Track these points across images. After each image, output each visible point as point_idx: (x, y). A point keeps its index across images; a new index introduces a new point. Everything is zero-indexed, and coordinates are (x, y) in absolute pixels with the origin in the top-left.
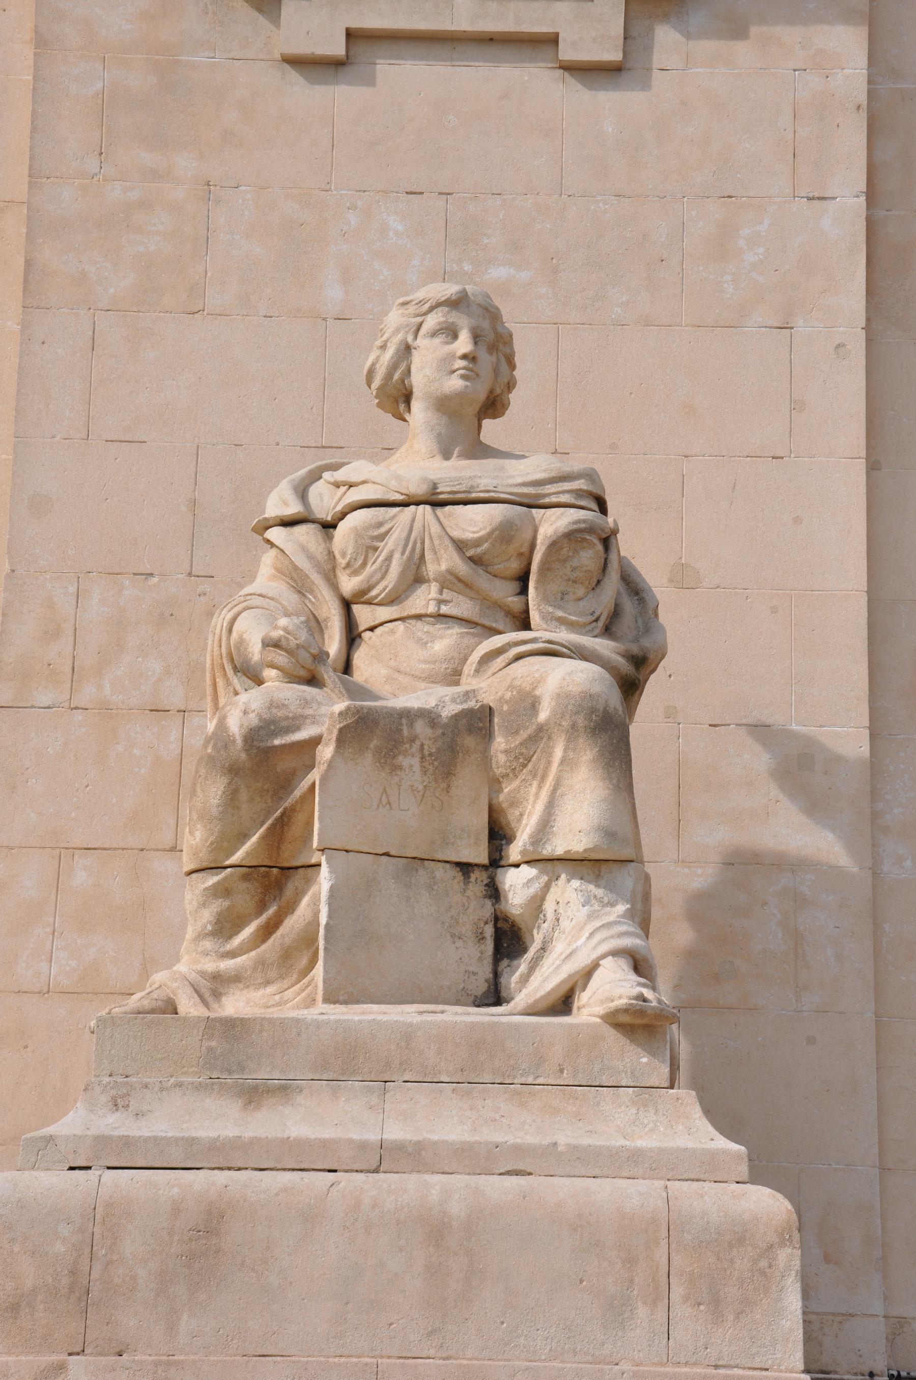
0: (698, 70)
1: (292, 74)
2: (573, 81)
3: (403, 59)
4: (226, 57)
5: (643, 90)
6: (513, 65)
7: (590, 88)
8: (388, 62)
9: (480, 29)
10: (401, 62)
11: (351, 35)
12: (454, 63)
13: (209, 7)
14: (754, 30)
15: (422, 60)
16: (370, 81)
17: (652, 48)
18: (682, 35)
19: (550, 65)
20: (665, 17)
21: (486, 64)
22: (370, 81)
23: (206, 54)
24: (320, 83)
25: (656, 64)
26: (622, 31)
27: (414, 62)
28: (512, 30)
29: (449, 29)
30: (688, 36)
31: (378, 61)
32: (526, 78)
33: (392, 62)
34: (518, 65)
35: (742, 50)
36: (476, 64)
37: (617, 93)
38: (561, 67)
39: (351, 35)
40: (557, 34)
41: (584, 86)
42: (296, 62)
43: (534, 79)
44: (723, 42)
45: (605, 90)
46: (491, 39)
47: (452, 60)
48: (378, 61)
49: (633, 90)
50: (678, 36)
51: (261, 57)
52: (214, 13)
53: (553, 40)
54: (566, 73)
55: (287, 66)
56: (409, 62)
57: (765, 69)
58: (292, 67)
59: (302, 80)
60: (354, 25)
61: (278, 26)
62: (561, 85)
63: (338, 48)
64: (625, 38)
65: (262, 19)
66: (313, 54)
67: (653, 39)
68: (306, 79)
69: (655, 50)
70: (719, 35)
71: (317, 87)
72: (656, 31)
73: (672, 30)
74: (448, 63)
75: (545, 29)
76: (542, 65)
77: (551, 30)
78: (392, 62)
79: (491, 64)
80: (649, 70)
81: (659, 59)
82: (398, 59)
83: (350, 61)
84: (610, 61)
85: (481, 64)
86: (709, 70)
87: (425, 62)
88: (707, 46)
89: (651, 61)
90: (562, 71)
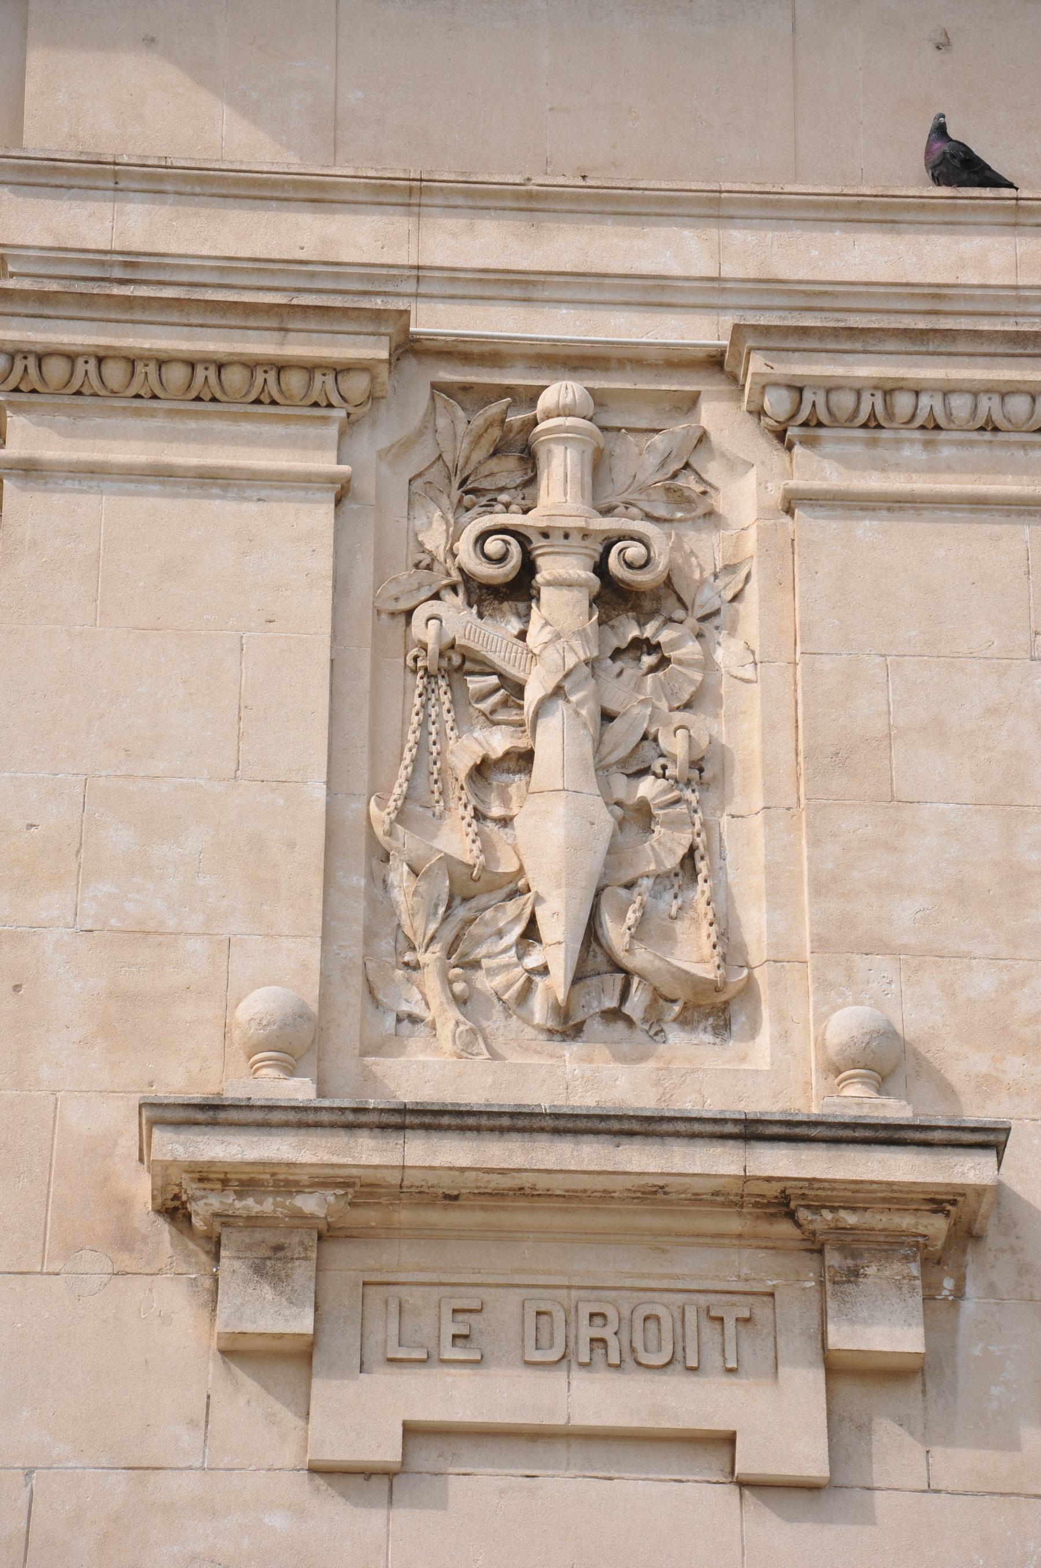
22: (441, 1504)
39: (411, 1431)
43: (700, 1500)
63: (388, 1450)
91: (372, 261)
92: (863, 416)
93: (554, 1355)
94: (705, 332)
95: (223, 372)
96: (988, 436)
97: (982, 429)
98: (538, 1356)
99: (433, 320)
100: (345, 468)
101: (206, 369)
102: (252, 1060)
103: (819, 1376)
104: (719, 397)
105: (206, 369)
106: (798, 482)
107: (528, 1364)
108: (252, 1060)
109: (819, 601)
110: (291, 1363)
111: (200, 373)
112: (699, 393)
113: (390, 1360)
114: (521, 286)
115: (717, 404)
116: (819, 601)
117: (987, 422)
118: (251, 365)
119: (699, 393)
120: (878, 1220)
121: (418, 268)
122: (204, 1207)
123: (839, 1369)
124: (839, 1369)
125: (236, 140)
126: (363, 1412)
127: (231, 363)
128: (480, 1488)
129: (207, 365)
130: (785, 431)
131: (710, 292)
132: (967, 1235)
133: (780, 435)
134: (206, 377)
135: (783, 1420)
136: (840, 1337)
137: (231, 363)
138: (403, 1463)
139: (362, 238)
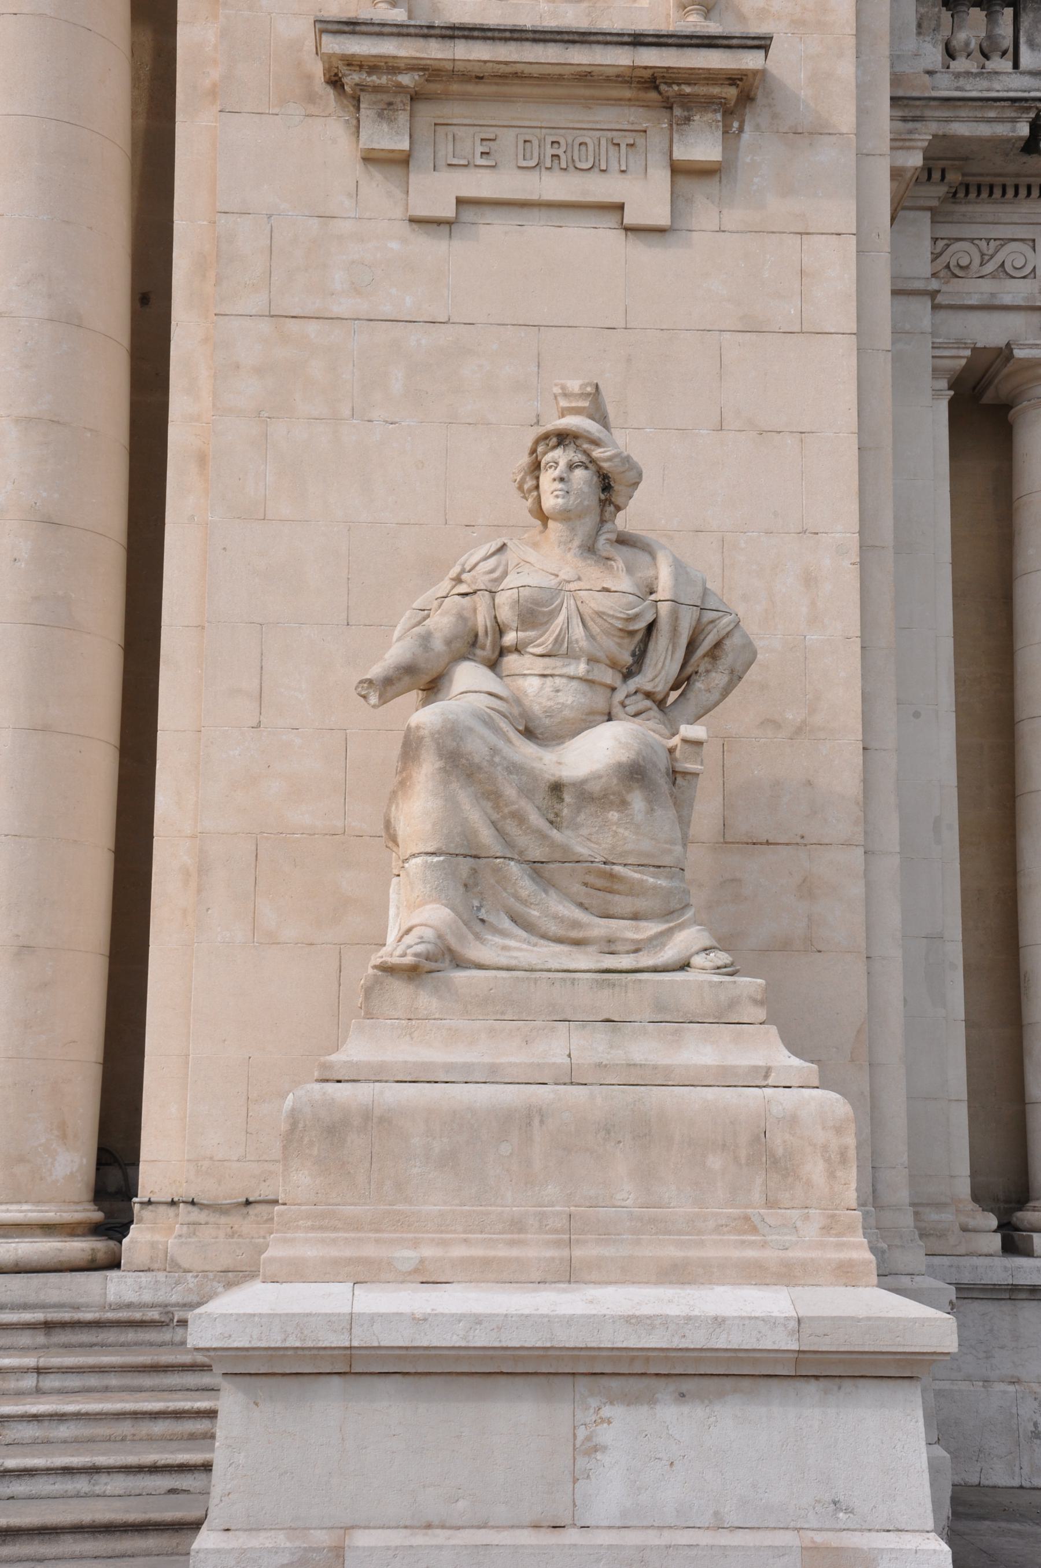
39: (460, 202)
43: (600, 238)
63: (448, 211)
126: (435, 191)
128: (495, 232)
132: (747, 98)
135: (648, 196)
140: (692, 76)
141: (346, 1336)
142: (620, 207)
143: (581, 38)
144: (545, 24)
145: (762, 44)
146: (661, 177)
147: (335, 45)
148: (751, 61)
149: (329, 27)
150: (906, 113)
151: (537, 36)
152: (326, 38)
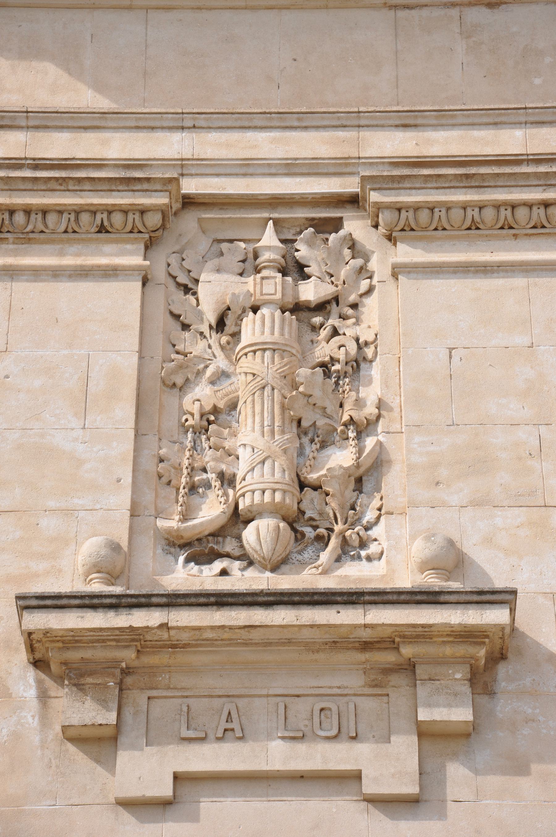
0: (488, 802)
1: (125, 815)
2: (377, 812)
3: (224, 796)
4: (66, 803)
5: (440, 819)
6: (322, 799)
7: (392, 818)
8: (211, 799)
9: (292, 769)
10: (222, 799)
11: (177, 777)
12: (269, 799)
13: (53, 761)
14: (535, 767)
15: (241, 796)
16: (195, 818)
17: (445, 783)
18: (470, 771)
19: (359, 798)
20: (454, 756)
21: (298, 798)
22: (195, 818)
23: (48, 802)
24: (149, 822)
25: (450, 797)
26: (417, 768)
27: (233, 799)
28: (319, 768)
29: (265, 769)
30: (477, 772)
31: (201, 800)
32: (334, 810)
33: (214, 799)
34: (326, 799)
35: (525, 784)
36: (289, 799)
37: (416, 823)
38: (365, 800)
39: (178, 778)
40: (360, 771)
41: (387, 816)
42: (128, 804)
43: (341, 811)
44: (508, 777)
45: (405, 819)
46: (302, 777)
47: (267, 796)
48: (201, 800)
49: (430, 819)
50: (467, 771)
51: (97, 801)
52: (58, 767)
53: (357, 776)
54: (370, 805)
55: (120, 808)
56: (229, 799)
57: (548, 802)
58: (124, 809)
59: (133, 820)
60: (181, 768)
61: (113, 773)
62: (366, 816)
63: (166, 790)
64: (420, 774)
65: (99, 769)
66: (144, 796)
67: (445, 775)
68: (128, 812)
69: (448, 784)
70: (504, 771)
71: (146, 825)
72: (448, 768)
73: (462, 767)
74: (264, 799)
75: (348, 767)
76: (348, 798)
77: (355, 768)
78: (214, 799)
79: (303, 799)
80: (444, 801)
81: (453, 791)
82: (219, 797)
83: (176, 801)
84: (409, 794)
85: (294, 799)
86: (498, 802)
87: (243, 799)
88: (494, 781)
89: (445, 794)
90: (366, 803)
91: (234, 157)
92: (468, 223)
93: (334, 732)
94: (349, 185)
95: (515, 210)
96: (440, 233)
97: (502, 228)
98: (191, 734)
99: (190, 186)
100: (148, 263)
101: (134, 214)
102: (90, 577)
103: (415, 738)
104: (352, 218)
105: (37, 214)
106: (400, 259)
107: (184, 739)
108: (90, 577)
109: (420, 321)
110: (100, 743)
111: (469, 212)
112: (341, 218)
113: (184, 739)
114: (247, 168)
115: (358, 221)
116: (420, 321)
117: (133, 228)
118: (125, 211)
119: (341, 218)
120: (99, 654)
121: (182, 160)
122: (55, 658)
123: (426, 734)
124: (426, 734)
125: (88, 98)
126: (146, 769)
127: (519, 205)
128: (219, 811)
129: (134, 212)
130: (391, 235)
131: (340, 167)
132: (499, 656)
133: (389, 238)
134: (3, 219)
135: (391, 763)
136: (423, 715)
137: (519, 205)
138: (174, 796)
139: (171, 146)
140: (422, 634)
141: (240, 705)
142: (357, 776)
143: (431, 598)
144: (492, 132)
145: (506, 597)
146: (405, 746)
147: (39, 621)
148: (496, 616)
149: (29, 603)
150: (485, 633)
151: (96, 601)
152: (26, 615)
